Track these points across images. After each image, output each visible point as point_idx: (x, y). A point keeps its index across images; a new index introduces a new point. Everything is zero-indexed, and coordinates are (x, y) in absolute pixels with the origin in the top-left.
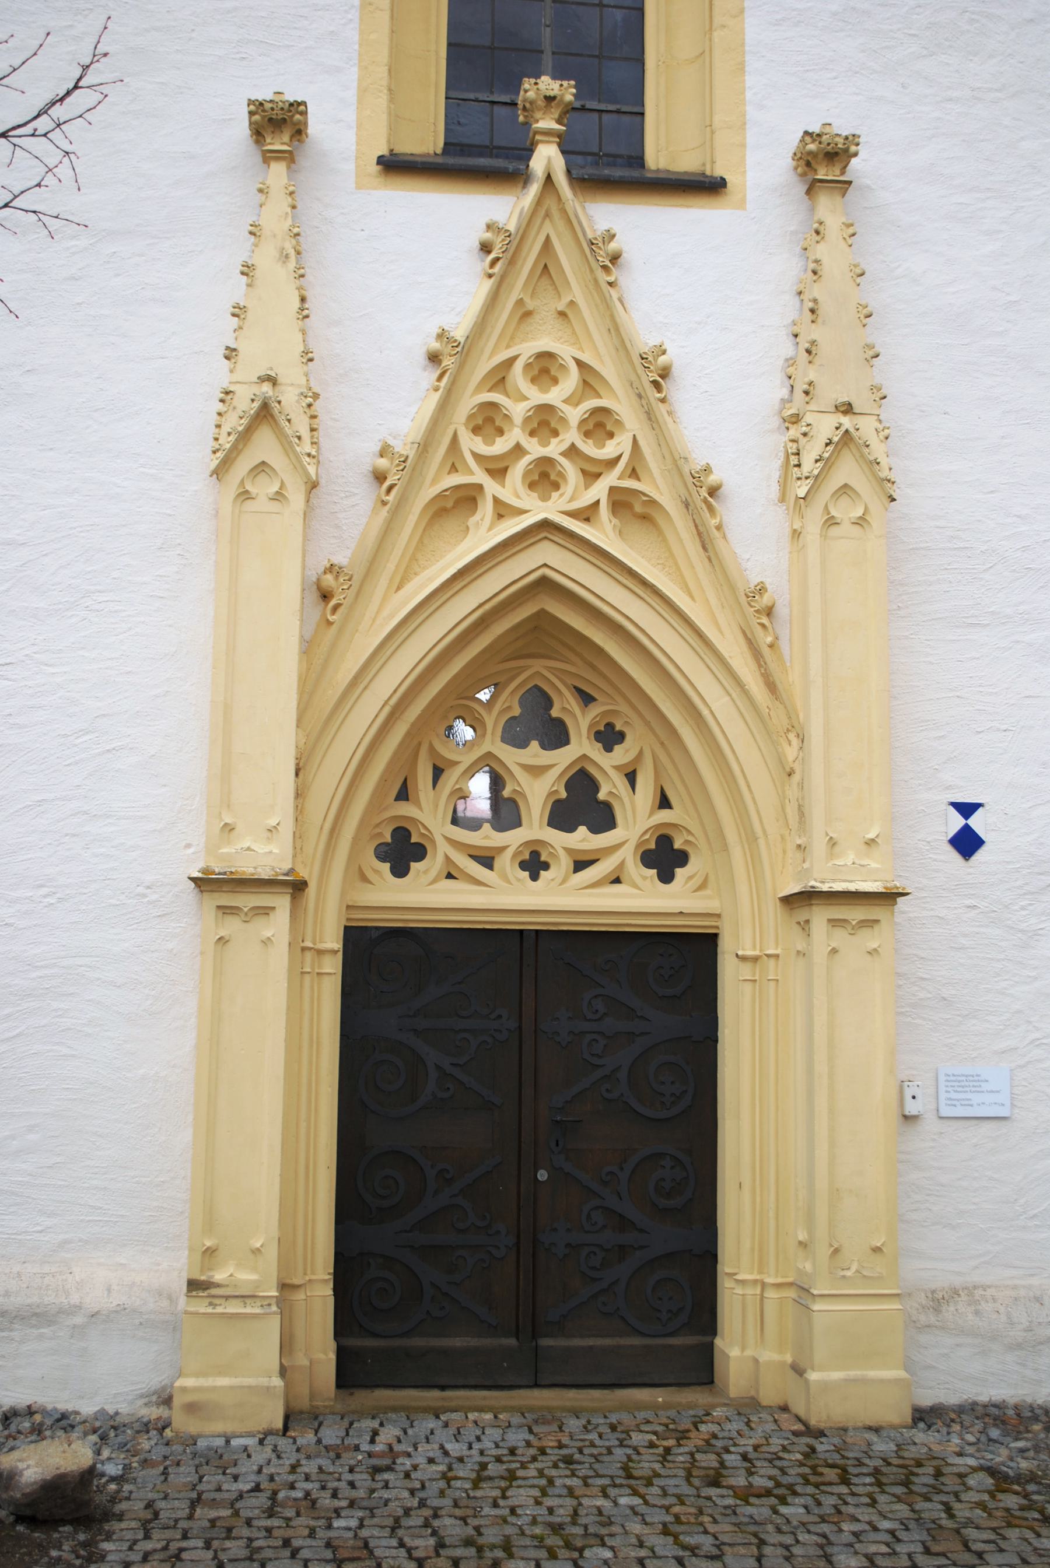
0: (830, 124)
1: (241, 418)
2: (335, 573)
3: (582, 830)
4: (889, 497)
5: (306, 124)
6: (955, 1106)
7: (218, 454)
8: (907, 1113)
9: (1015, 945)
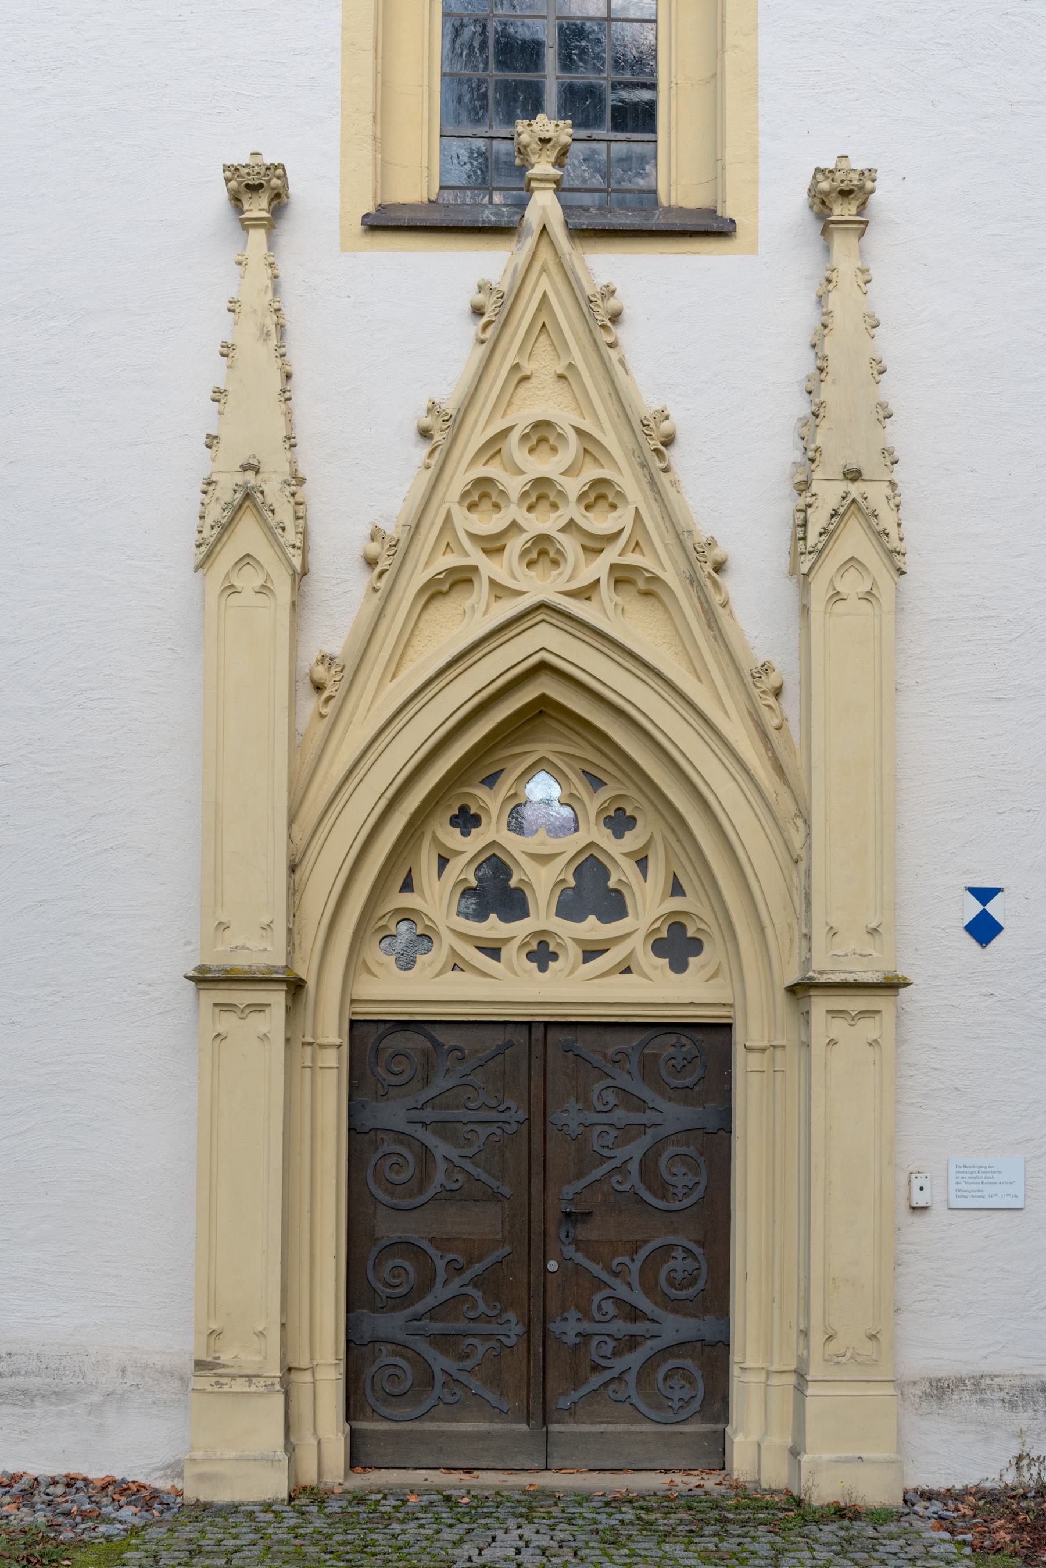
0: (847, 157)
1: (224, 510)
2: (327, 665)
3: (592, 919)
4: (898, 570)
5: (286, 186)
6: (966, 1197)
7: (202, 549)
8: (914, 1205)
9: (1034, 1034)
